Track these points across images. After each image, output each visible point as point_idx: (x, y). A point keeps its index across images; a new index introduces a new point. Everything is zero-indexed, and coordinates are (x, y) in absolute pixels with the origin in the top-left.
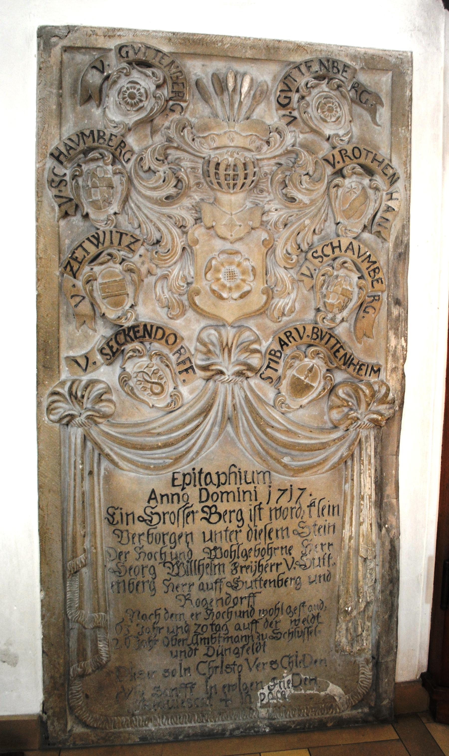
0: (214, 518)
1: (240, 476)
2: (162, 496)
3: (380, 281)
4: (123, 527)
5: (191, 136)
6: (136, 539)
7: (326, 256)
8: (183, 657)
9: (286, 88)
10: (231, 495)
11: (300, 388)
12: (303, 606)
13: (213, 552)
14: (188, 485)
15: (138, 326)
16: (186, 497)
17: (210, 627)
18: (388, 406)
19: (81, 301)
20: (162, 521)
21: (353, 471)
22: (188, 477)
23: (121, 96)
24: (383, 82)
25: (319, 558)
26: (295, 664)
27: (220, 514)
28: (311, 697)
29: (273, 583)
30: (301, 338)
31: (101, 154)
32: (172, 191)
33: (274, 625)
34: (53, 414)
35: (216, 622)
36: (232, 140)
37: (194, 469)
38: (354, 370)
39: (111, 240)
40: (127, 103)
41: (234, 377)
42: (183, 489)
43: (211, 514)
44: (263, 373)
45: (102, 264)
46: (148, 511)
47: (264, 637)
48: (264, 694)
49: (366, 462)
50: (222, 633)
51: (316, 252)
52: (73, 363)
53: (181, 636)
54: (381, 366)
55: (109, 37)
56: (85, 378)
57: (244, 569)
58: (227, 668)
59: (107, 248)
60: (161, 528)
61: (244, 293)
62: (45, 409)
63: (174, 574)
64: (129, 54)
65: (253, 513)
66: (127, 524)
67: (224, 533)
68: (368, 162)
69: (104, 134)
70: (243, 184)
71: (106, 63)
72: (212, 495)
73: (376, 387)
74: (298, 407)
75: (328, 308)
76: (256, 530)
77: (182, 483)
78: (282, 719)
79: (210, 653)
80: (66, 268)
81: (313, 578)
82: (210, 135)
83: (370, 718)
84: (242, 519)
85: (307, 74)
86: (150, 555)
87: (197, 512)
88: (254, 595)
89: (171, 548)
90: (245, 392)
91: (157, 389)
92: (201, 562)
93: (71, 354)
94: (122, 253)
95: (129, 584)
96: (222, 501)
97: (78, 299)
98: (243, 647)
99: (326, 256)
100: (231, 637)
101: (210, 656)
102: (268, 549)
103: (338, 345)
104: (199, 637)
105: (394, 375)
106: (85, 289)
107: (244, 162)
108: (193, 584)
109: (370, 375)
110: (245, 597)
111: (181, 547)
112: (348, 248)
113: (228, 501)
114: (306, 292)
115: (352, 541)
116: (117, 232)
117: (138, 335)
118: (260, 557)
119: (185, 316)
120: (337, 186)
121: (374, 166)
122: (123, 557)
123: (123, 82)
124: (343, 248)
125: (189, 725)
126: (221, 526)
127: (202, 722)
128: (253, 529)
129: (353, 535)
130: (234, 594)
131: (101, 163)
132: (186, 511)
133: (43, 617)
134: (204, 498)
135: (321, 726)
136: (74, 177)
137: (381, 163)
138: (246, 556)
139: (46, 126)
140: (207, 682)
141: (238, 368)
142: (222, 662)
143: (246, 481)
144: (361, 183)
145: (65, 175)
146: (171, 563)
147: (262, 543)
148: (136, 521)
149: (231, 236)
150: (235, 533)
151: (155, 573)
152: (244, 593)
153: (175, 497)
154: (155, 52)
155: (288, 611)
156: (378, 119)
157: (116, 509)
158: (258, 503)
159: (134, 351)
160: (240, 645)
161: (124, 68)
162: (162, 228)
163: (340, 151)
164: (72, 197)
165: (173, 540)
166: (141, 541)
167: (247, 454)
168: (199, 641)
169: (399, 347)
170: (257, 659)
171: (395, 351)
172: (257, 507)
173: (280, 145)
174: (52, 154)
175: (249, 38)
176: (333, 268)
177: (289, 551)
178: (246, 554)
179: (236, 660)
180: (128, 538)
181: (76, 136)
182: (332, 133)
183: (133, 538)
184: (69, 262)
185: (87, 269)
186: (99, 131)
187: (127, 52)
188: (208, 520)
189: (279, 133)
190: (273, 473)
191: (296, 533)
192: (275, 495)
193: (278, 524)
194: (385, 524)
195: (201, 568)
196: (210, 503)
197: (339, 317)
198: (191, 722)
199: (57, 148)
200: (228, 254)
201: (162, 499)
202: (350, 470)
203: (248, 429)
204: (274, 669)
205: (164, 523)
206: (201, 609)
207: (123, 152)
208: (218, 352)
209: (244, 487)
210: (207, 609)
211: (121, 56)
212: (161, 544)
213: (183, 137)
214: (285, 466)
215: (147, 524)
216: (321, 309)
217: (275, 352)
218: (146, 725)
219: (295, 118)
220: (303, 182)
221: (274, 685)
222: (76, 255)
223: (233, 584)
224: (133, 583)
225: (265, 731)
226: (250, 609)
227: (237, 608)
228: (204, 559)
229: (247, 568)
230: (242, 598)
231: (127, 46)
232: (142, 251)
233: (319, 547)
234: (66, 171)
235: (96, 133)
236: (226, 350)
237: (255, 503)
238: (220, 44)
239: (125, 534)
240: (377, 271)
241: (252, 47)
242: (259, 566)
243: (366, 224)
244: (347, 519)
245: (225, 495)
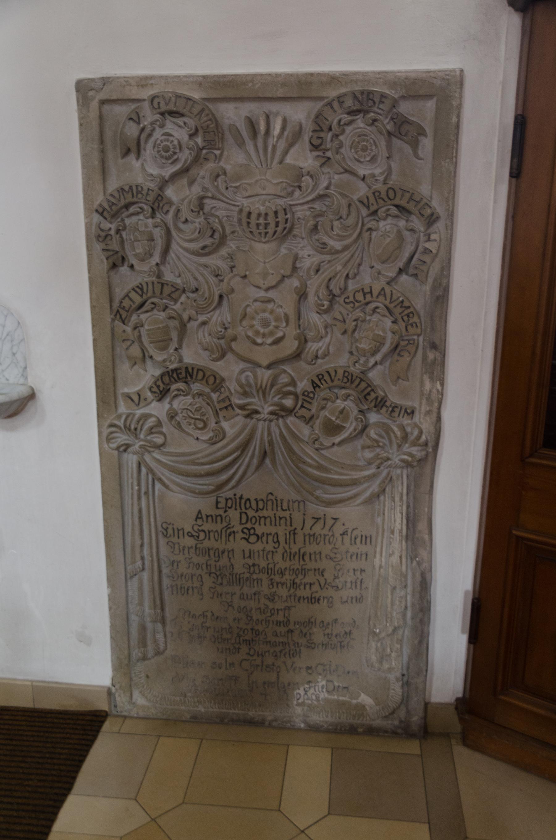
0: (253, 539)
1: (277, 503)
2: (207, 516)
3: (414, 325)
4: (175, 540)
5: (224, 185)
6: (186, 551)
7: (357, 301)
9: (318, 128)
10: (268, 521)
11: (332, 429)
12: (335, 622)
13: (252, 568)
14: (229, 508)
15: (180, 369)
16: (228, 518)
17: (250, 631)
18: (420, 448)
19: (131, 345)
20: (207, 537)
21: (384, 506)
22: (230, 503)
23: (156, 149)
24: (424, 112)
25: (351, 582)
26: (328, 672)
28: (343, 703)
30: (332, 381)
31: (141, 208)
32: (208, 241)
34: (112, 443)
35: (256, 628)
36: (264, 189)
37: (235, 495)
38: (387, 411)
39: (154, 290)
40: (162, 157)
41: (268, 415)
42: (225, 511)
43: (250, 535)
44: (297, 412)
45: (147, 312)
46: (196, 528)
47: (300, 645)
48: (300, 694)
49: (397, 499)
51: (348, 297)
52: (128, 399)
53: (226, 636)
54: (415, 408)
55: (142, 86)
56: (139, 412)
57: (280, 585)
58: (267, 667)
59: (150, 298)
60: (207, 544)
61: (277, 338)
62: (105, 438)
63: (218, 583)
64: (161, 105)
66: (179, 538)
67: (261, 553)
68: (403, 203)
69: (142, 188)
70: (275, 232)
71: (141, 115)
72: (251, 519)
73: (409, 429)
74: (330, 444)
75: (360, 352)
76: (290, 553)
77: (224, 506)
78: (316, 718)
79: (252, 652)
80: (116, 315)
81: (345, 599)
82: (241, 185)
83: (400, 731)
84: (278, 541)
85: (339, 111)
86: (198, 566)
87: (238, 532)
88: (289, 608)
89: (215, 561)
90: (280, 429)
91: (201, 425)
92: (241, 576)
93: (126, 390)
94: (164, 301)
95: (181, 588)
96: (260, 524)
97: (128, 343)
98: (281, 652)
99: (357, 301)
101: (252, 656)
102: (302, 569)
103: (369, 389)
104: (241, 639)
105: (428, 418)
106: (134, 335)
107: (274, 210)
108: (235, 594)
109: (403, 417)
110: (281, 609)
111: (224, 561)
112: (379, 294)
113: (265, 525)
114: (339, 335)
115: (382, 570)
116: (158, 283)
119: (225, 358)
120: (370, 229)
121: (411, 206)
123: (158, 134)
124: (375, 294)
125: (233, 711)
126: (259, 546)
127: (245, 710)
128: (288, 551)
129: (383, 564)
131: (141, 217)
132: (228, 531)
133: (110, 609)
134: (244, 521)
135: (352, 730)
136: (118, 231)
137: (418, 202)
138: (282, 573)
139: (91, 182)
141: (271, 408)
142: (263, 662)
143: (282, 509)
144: (396, 225)
145: (110, 229)
146: (216, 574)
147: (296, 564)
148: (186, 536)
149: (264, 284)
150: (271, 553)
151: (202, 581)
152: (279, 605)
153: (219, 518)
154: (185, 100)
155: (321, 625)
156: (420, 153)
158: (293, 528)
159: (178, 390)
160: (278, 649)
161: (157, 121)
162: (200, 278)
163: (374, 193)
164: (117, 250)
165: (217, 555)
167: (283, 484)
168: (241, 642)
169: (434, 391)
171: (430, 394)
172: (292, 532)
173: (312, 190)
174: (97, 211)
175: (280, 75)
176: (365, 313)
177: (322, 573)
178: (281, 573)
180: (180, 549)
181: (117, 192)
182: (367, 173)
184: (118, 311)
185: (134, 318)
186: (137, 186)
187: (159, 103)
188: (247, 540)
189: (311, 177)
190: (306, 502)
191: (328, 557)
192: (309, 522)
194: (416, 557)
195: (241, 580)
196: (249, 525)
197: (372, 361)
198: (235, 709)
199: (100, 205)
200: (263, 302)
202: (382, 505)
203: (283, 462)
204: (310, 674)
205: (209, 539)
207: (161, 205)
208: (255, 393)
209: (280, 513)
210: (247, 616)
211: (154, 108)
213: (217, 187)
214: (317, 498)
215: (195, 539)
216: (354, 352)
217: (309, 393)
218: (197, 707)
219: (329, 159)
220: (335, 228)
221: (310, 688)
222: (124, 304)
223: (269, 596)
225: (300, 726)
226: (285, 620)
228: (244, 573)
229: (283, 584)
230: (278, 610)
231: (158, 97)
232: (183, 298)
233: (351, 572)
234: (110, 226)
235: (134, 188)
236: (261, 392)
237: (289, 528)
238: (250, 84)
239: (177, 546)
240: (411, 315)
241: (284, 85)
242: (294, 584)
243: (401, 268)
244: (378, 549)
245: (263, 520)
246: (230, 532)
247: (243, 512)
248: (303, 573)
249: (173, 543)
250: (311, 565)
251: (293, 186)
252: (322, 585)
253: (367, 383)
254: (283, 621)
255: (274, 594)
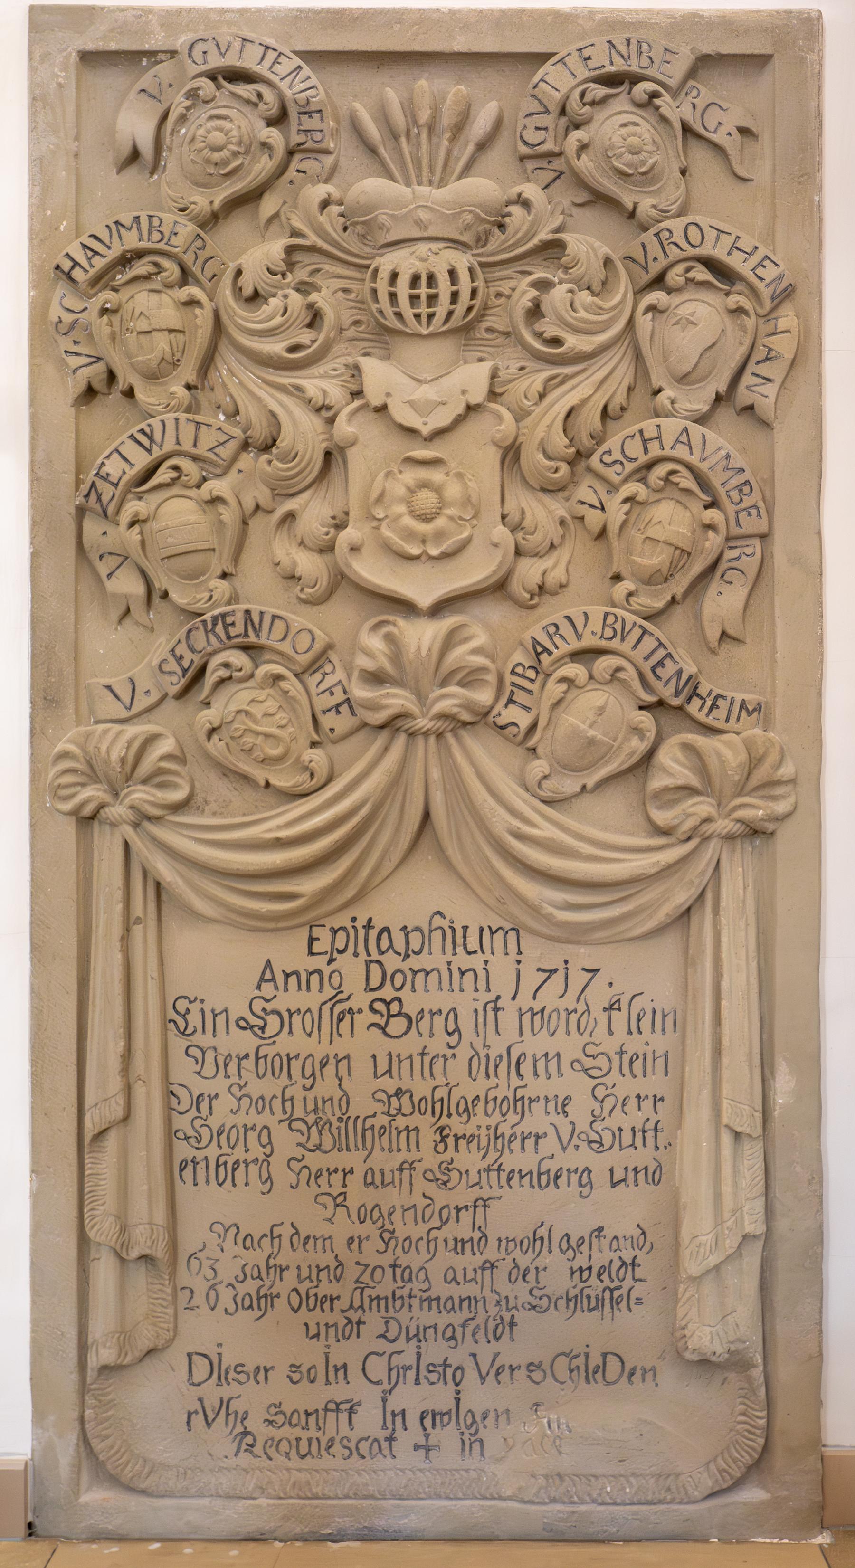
0: (397, 1026)
2: (287, 976)
4: (205, 1040)
6: (233, 1068)
8: (332, 1339)
14: (340, 952)
17: (389, 1272)
20: (286, 1028)
27: (409, 1018)
29: (527, 1179)
30: (579, 637)
31: (156, 264)
33: (531, 1277)
35: (404, 1261)
37: (354, 919)
42: (331, 961)
43: (390, 1016)
46: (258, 1006)
50: (416, 1286)
53: (326, 1289)
57: (462, 1143)
60: (285, 1044)
65: (481, 1020)
67: (417, 1060)
70: (450, 313)
76: (487, 1057)
81: (619, 1175)
84: (457, 1030)
86: (261, 1104)
95: (218, 1166)
100: (438, 1299)
101: (393, 1341)
103: (662, 652)
104: (367, 1292)
111: (327, 1087)
117: (233, 632)
118: (497, 1117)
122: (204, 1106)
126: (411, 1044)
128: (483, 1053)
130: (441, 1197)
132: (338, 1009)
134: (375, 982)
140: (384, 1400)
142: (419, 1355)
143: (465, 947)
146: (306, 1123)
147: (503, 1086)
150: (442, 1060)
153: (315, 978)
157: (191, 1002)
158: (492, 996)
160: (457, 1318)
165: (308, 1072)
166: (243, 1072)
170: (497, 1355)
172: (491, 1006)
177: (563, 1106)
178: (466, 1110)
179: (450, 1353)
183: (226, 1065)
184: (93, 484)
188: (383, 1029)
193: (536, 1044)
195: (369, 1134)
196: (388, 993)
201: (286, 983)
205: (291, 1032)
206: (369, 1229)
209: (462, 960)
212: (284, 1080)
215: (256, 1035)
222: (106, 469)
224: (225, 1163)
226: (477, 1235)
227: (449, 1232)
228: (374, 1115)
230: (458, 1210)
240: (746, 489)
242: (496, 1138)
246: (342, 1012)
247: (371, 961)
248: (519, 1110)
249: (201, 1049)
250: (535, 1087)
251: (489, 222)
252: (565, 1140)
253: (657, 639)
254: (472, 1239)
255: (447, 1167)
